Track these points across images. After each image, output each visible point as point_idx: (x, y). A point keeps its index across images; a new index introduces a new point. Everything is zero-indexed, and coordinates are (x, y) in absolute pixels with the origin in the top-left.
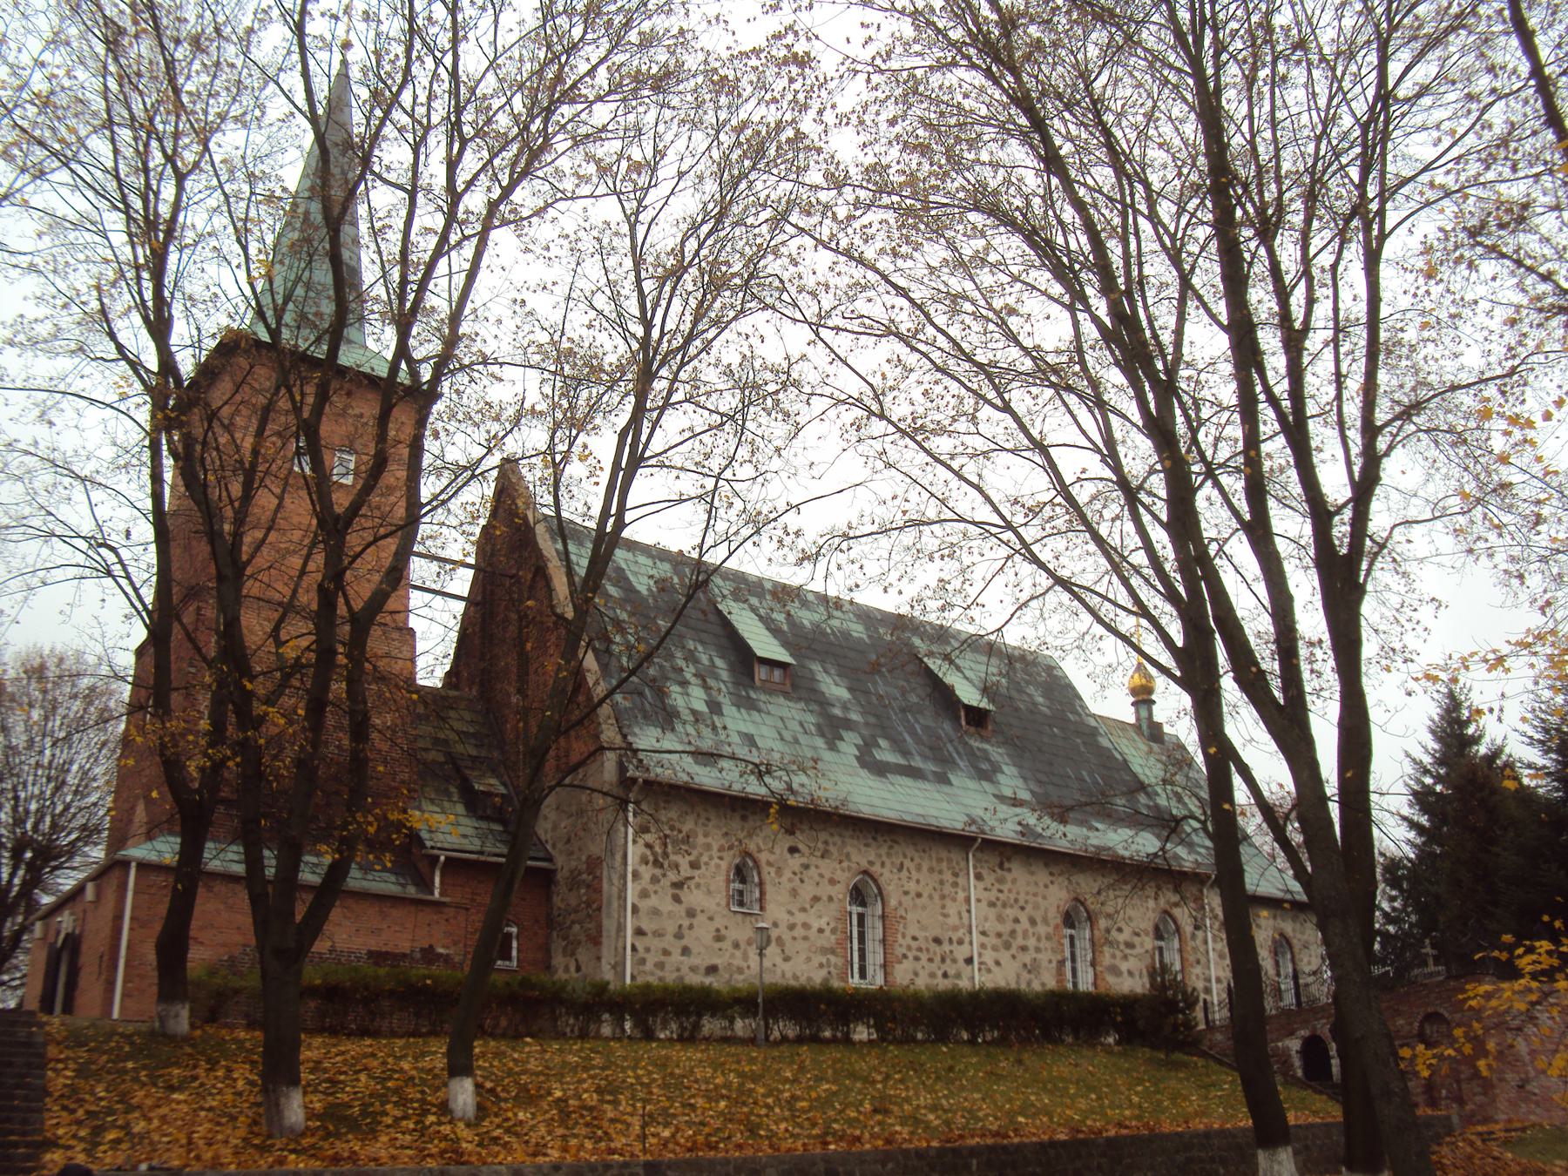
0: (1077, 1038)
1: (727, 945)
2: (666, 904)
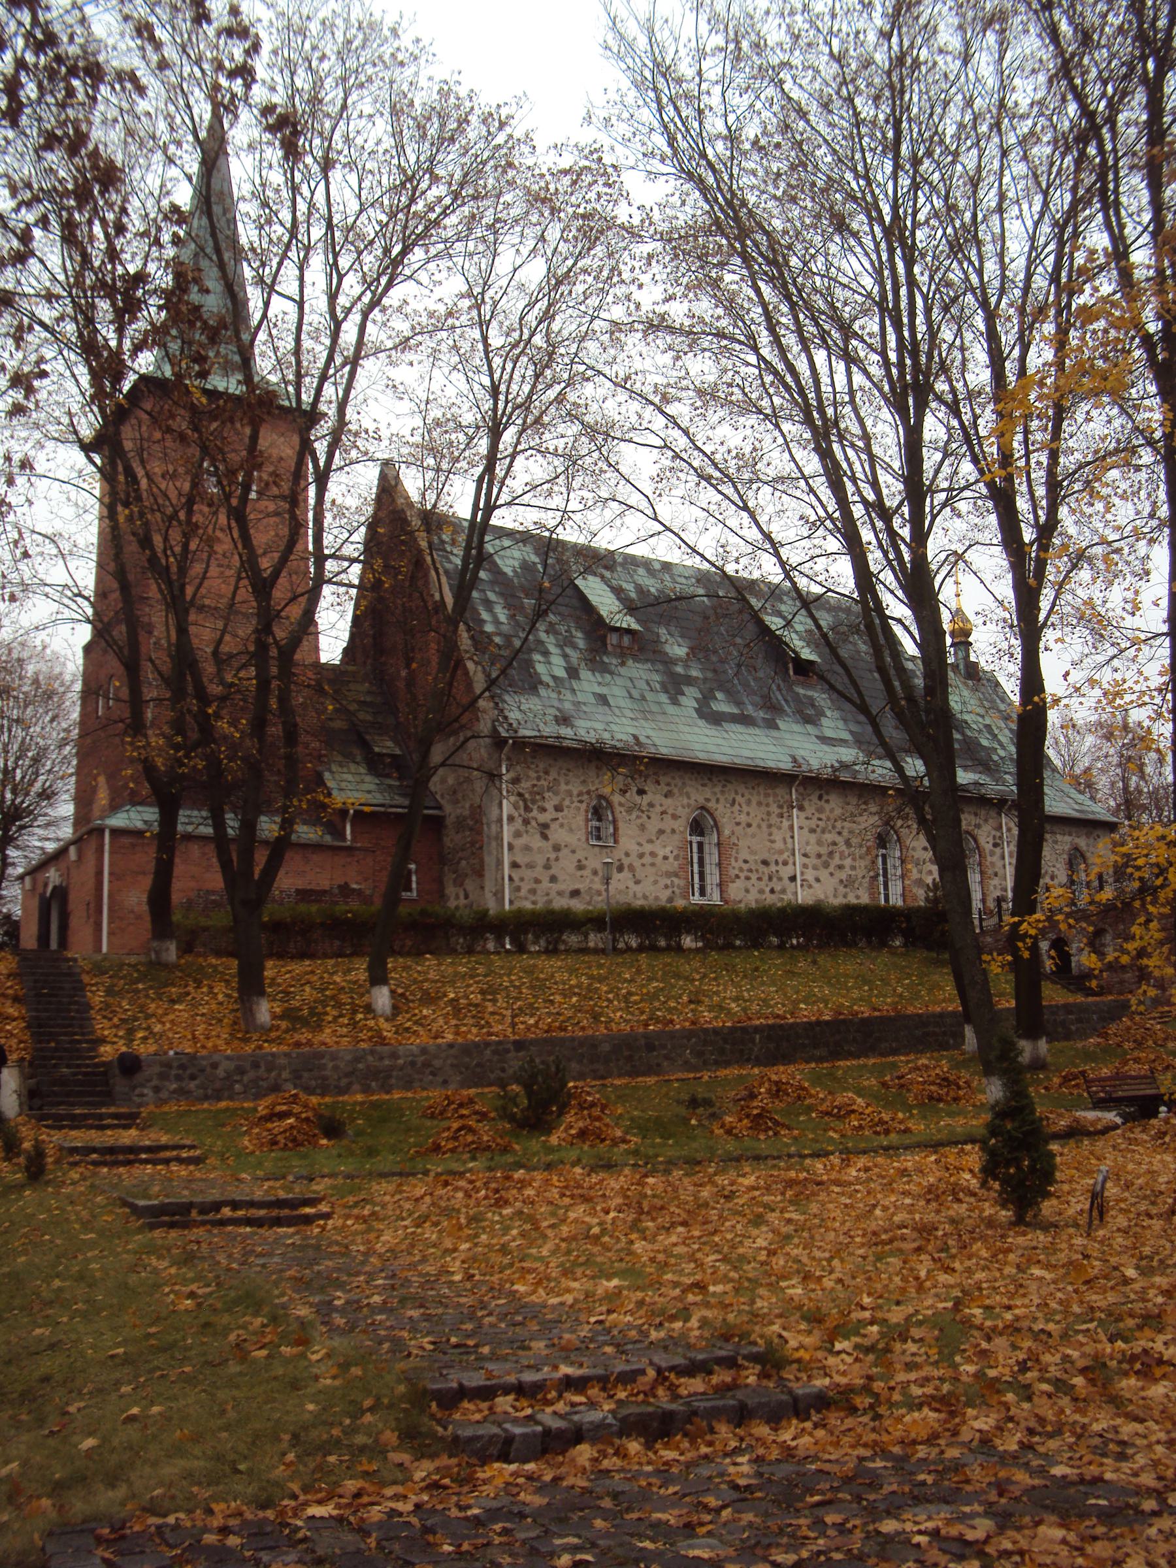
0: (869, 942)
1: (587, 873)
2: (536, 842)
